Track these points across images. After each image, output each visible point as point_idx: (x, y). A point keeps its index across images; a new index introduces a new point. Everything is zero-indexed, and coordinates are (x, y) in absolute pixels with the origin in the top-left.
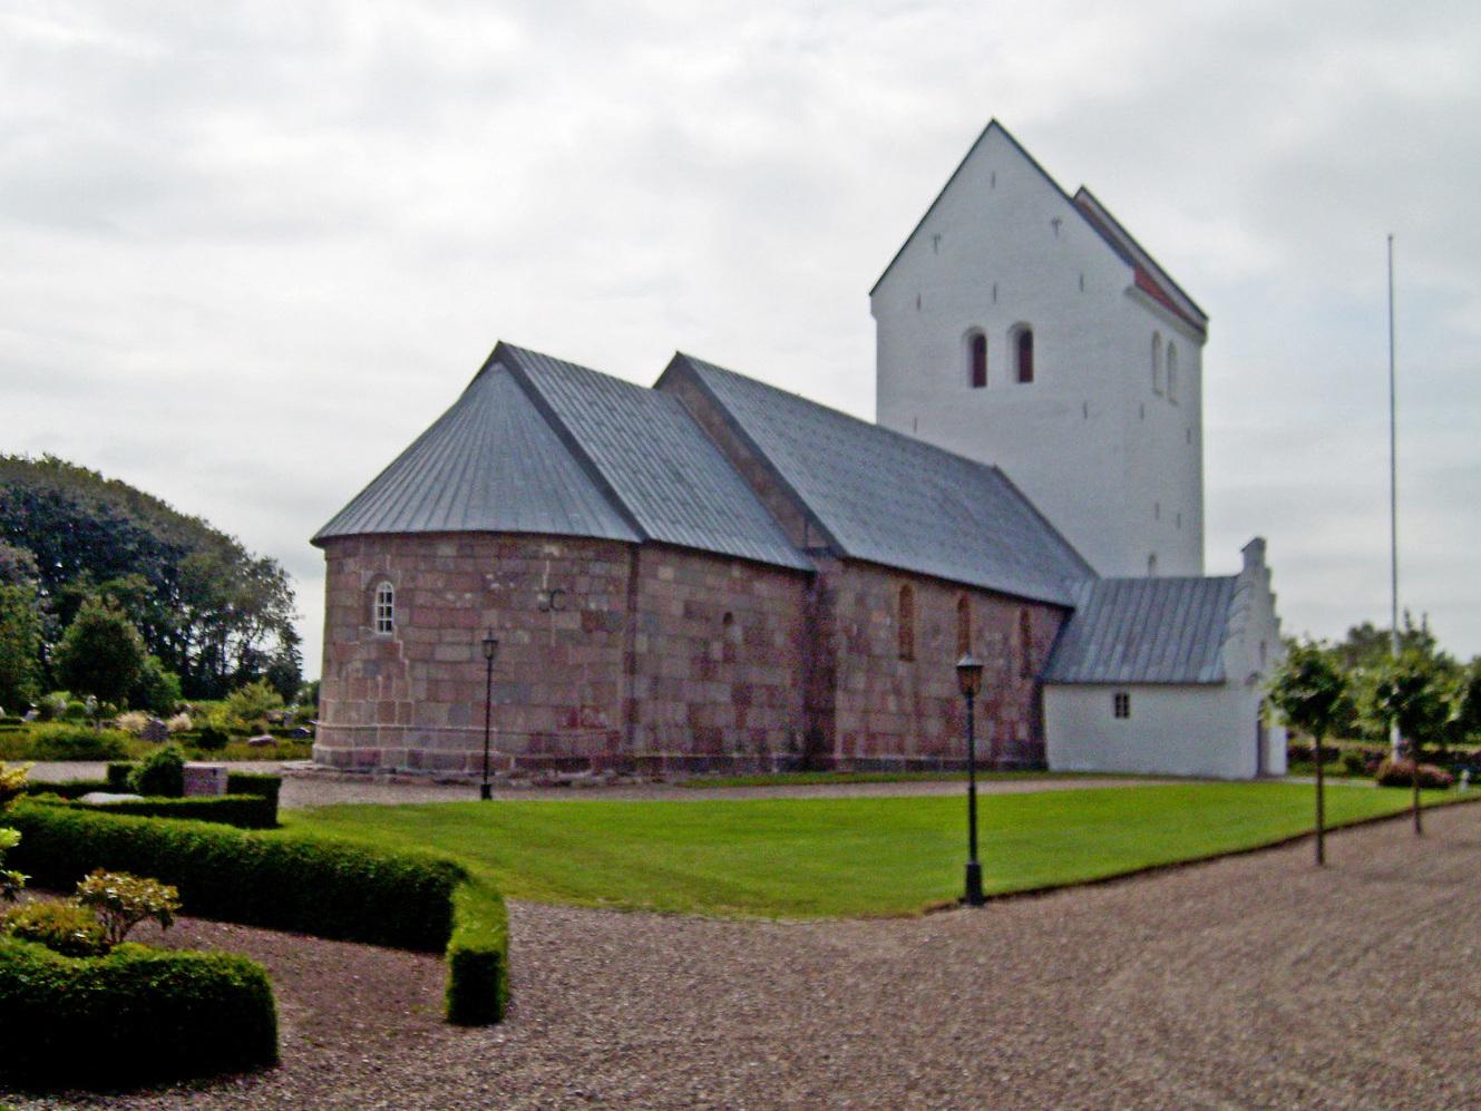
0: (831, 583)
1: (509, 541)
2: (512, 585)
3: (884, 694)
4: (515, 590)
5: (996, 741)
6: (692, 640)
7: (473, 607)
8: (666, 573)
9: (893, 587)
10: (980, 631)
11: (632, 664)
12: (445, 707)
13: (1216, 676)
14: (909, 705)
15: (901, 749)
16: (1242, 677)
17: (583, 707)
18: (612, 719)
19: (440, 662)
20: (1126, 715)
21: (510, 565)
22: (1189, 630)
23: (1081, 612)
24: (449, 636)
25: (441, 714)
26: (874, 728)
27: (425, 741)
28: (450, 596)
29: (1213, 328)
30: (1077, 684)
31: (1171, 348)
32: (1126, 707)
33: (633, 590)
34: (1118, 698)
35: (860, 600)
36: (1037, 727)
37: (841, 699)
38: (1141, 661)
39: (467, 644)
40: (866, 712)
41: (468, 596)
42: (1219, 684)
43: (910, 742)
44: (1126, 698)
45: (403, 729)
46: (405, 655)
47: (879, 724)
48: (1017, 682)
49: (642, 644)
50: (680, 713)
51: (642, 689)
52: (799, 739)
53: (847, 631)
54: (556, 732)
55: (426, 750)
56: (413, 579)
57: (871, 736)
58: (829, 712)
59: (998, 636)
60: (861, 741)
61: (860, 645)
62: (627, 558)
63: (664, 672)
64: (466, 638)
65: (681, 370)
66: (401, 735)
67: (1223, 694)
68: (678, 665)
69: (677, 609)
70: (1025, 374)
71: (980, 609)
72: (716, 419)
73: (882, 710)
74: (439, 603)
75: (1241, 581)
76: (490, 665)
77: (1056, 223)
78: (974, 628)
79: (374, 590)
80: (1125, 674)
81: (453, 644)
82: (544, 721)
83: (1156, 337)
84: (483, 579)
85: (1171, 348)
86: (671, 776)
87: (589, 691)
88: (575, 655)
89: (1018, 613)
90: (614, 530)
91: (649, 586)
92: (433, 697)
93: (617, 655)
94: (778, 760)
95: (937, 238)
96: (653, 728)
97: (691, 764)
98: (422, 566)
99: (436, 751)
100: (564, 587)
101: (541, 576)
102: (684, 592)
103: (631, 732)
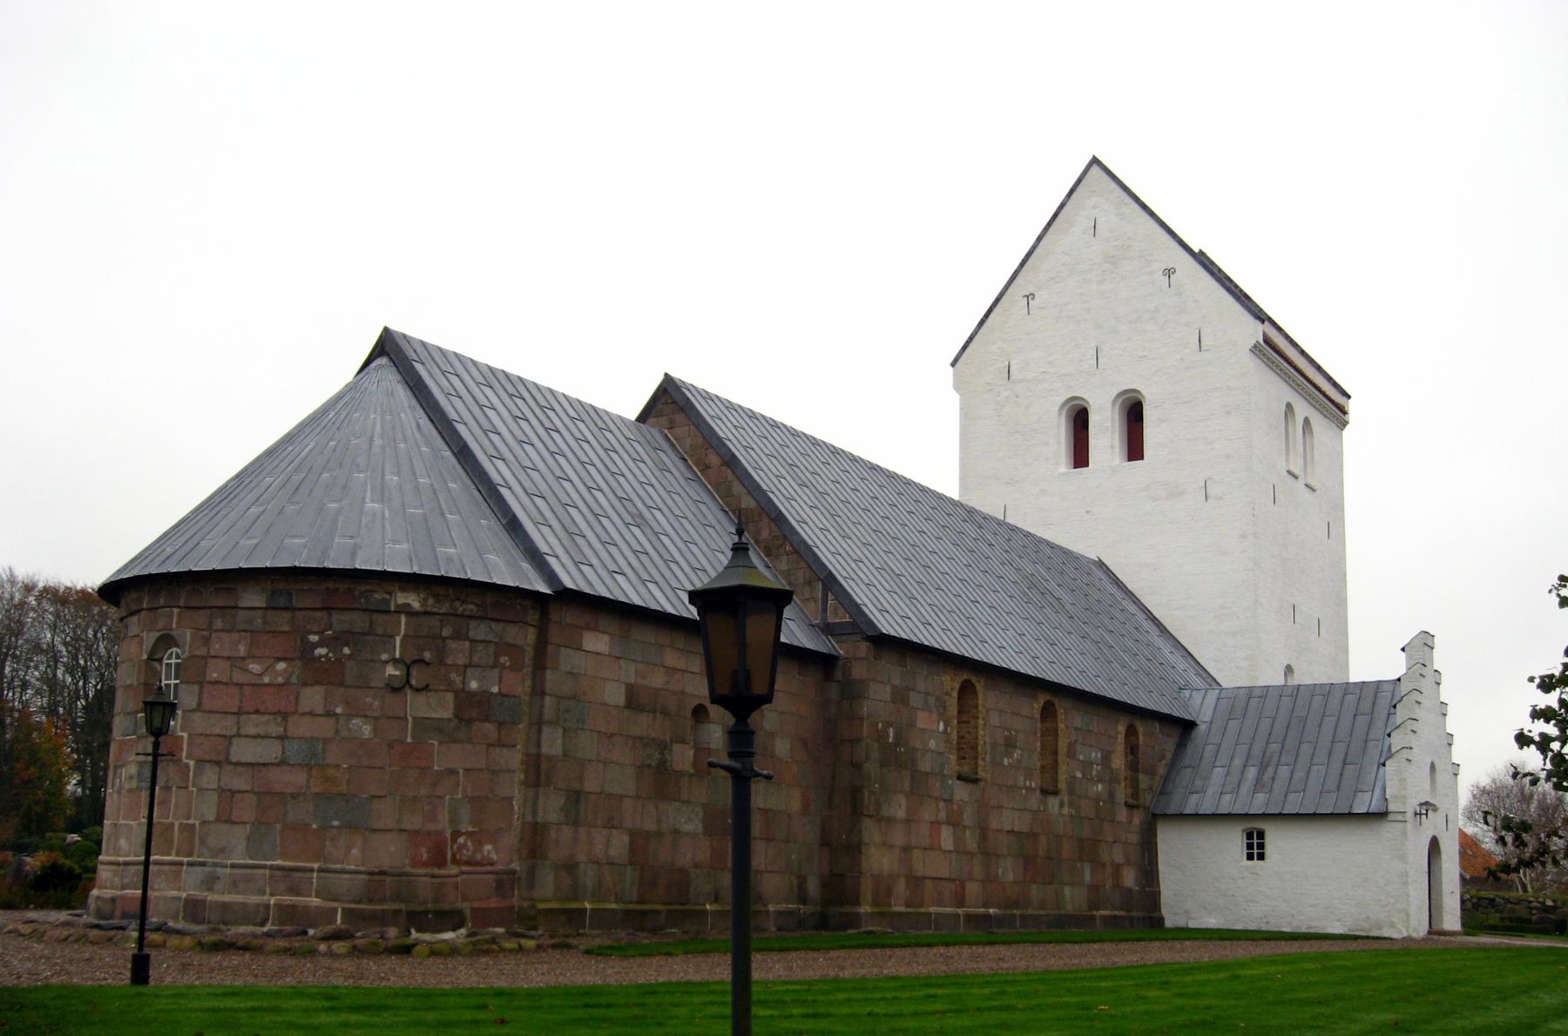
0: (858, 671)
1: (343, 586)
2: (346, 651)
3: (936, 824)
4: (350, 657)
5: (1094, 889)
6: (640, 741)
7: (287, 683)
8: (597, 642)
9: (950, 683)
10: (1071, 746)
11: (537, 772)
12: (241, 832)
13: (1375, 807)
14: (971, 841)
15: (961, 903)
16: (1412, 805)
17: (456, 834)
18: (500, 853)
19: (238, 764)
20: (1261, 857)
21: (342, 621)
22: (1340, 748)
23: (1202, 727)
24: (251, 726)
25: (236, 839)
26: (919, 869)
27: (209, 883)
28: (255, 667)
29: (1352, 406)
30: (1198, 817)
31: (1307, 421)
32: (1261, 846)
33: (540, 662)
34: (1250, 836)
35: (900, 697)
36: (1150, 874)
37: (871, 832)
38: (1279, 786)
39: (278, 737)
40: (907, 849)
41: (281, 666)
42: (1381, 816)
43: (973, 889)
44: (1261, 835)
45: (181, 864)
46: (189, 756)
47: (925, 864)
48: (1122, 814)
49: (553, 743)
50: (619, 845)
51: (551, 807)
52: (813, 887)
53: (881, 736)
54: (409, 869)
55: (211, 897)
56: (206, 641)
57: (915, 881)
58: (854, 849)
59: (1095, 755)
60: (901, 887)
61: (898, 756)
62: (532, 616)
63: (591, 785)
64: (276, 730)
65: (671, 404)
66: (180, 872)
67: (1387, 830)
68: (614, 774)
69: (615, 695)
70: (1135, 450)
71: (1070, 720)
72: (714, 460)
73: (934, 847)
74: (239, 677)
75: (1404, 688)
76: (156, 745)
77: (1169, 272)
78: (1063, 745)
79: (160, 661)
80: (1259, 804)
81: (256, 737)
82: (390, 852)
83: (1289, 406)
84: (304, 640)
85: (1307, 421)
86: (595, 938)
87: (465, 813)
88: (443, 757)
89: (1121, 728)
90: (505, 570)
91: (568, 659)
92: (225, 818)
93: (513, 758)
94: (779, 913)
95: (1030, 297)
96: (570, 867)
97: (636, 920)
98: (218, 624)
99: (227, 898)
100: (427, 656)
101: (392, 637)
102: (629, 672)
103: (532, 872)
